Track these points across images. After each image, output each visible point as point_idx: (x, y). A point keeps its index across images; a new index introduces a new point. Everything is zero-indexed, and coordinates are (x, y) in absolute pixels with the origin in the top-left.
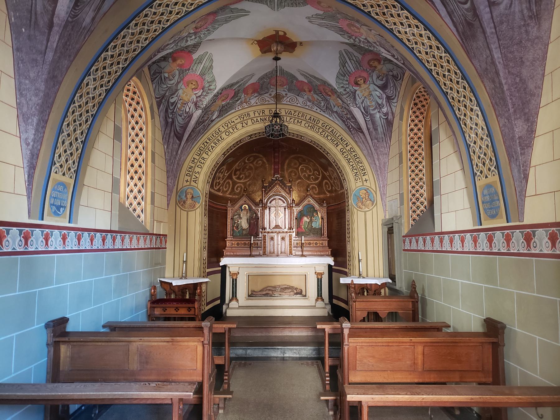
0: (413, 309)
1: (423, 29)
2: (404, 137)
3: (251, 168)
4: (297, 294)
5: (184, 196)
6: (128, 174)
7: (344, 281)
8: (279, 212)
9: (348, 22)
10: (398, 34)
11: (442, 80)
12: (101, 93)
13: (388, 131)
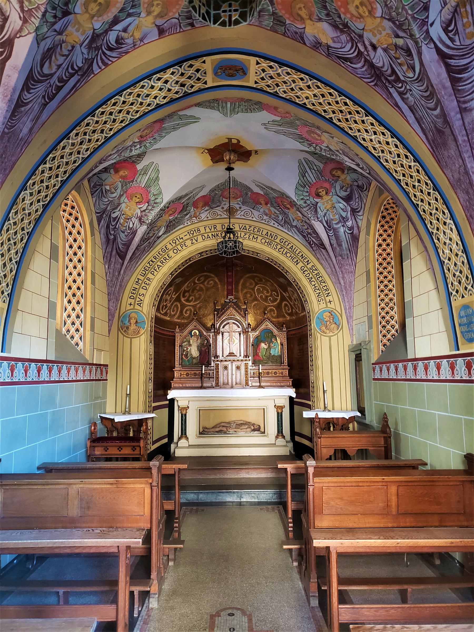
0: (385, 445)
1: (390, 136)
2: (371, 253)
3: (201, 289)
4: (254, 430)
5: (127, 321)
6: (66, 297)
7: (307, 415)
8: (234, 337)
9: (308, 129)
10: (362, 142)
11: (412, 191)
12: (38, 209)
13: (353, 247)
